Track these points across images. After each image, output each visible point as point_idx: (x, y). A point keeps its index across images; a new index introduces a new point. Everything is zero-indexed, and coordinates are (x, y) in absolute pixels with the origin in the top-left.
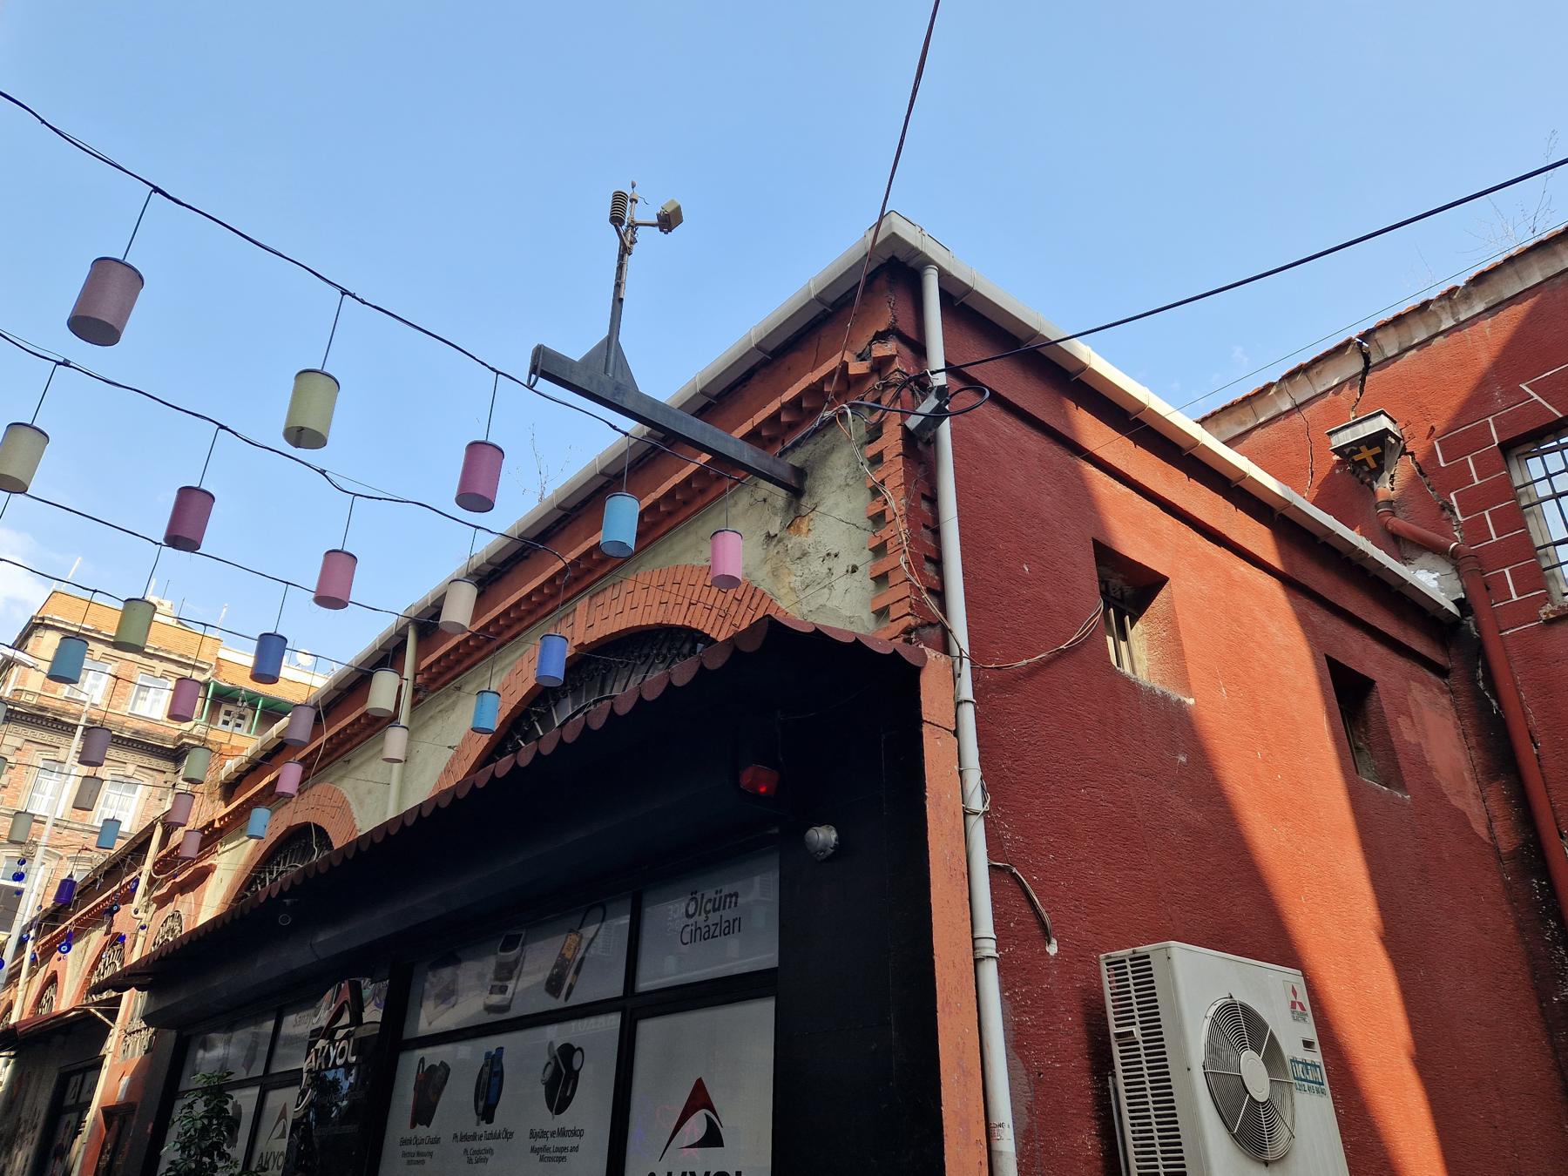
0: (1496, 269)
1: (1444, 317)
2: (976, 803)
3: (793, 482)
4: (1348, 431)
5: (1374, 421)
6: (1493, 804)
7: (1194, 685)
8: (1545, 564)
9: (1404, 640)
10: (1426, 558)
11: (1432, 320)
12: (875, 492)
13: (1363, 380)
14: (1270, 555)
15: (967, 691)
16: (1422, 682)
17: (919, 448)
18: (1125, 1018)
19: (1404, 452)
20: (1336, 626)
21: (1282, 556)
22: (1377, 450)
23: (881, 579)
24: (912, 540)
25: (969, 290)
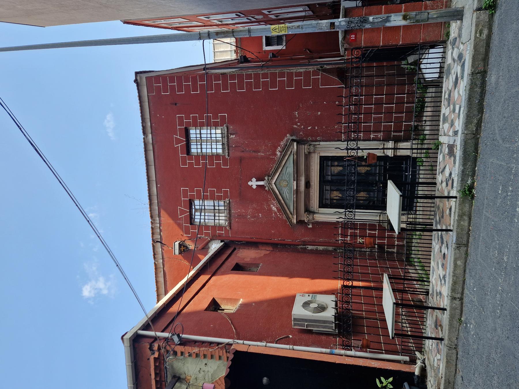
0: (151, 214)
1: (156, 225)
2: (264, 344)
3: (177, 379)
4: (175, 251)
5: (176, 245)
6: (263, 248)
7: (238, 298)
8: (218, 225)
9: (228, 254)
10: (210, 244)
11: (156, 227)
12: (190, 355)
13: (163, 244)
14: (207, 277)
15: (241, 342)
16: (237, 254)
17: (184, 343)
18: (303, 325)
19: (184, 241)
20: (224, 267)
21: (207, 274)
22: (182, 246)
23: (212, 357)
24: (206, 347)
25: (144, 325)
